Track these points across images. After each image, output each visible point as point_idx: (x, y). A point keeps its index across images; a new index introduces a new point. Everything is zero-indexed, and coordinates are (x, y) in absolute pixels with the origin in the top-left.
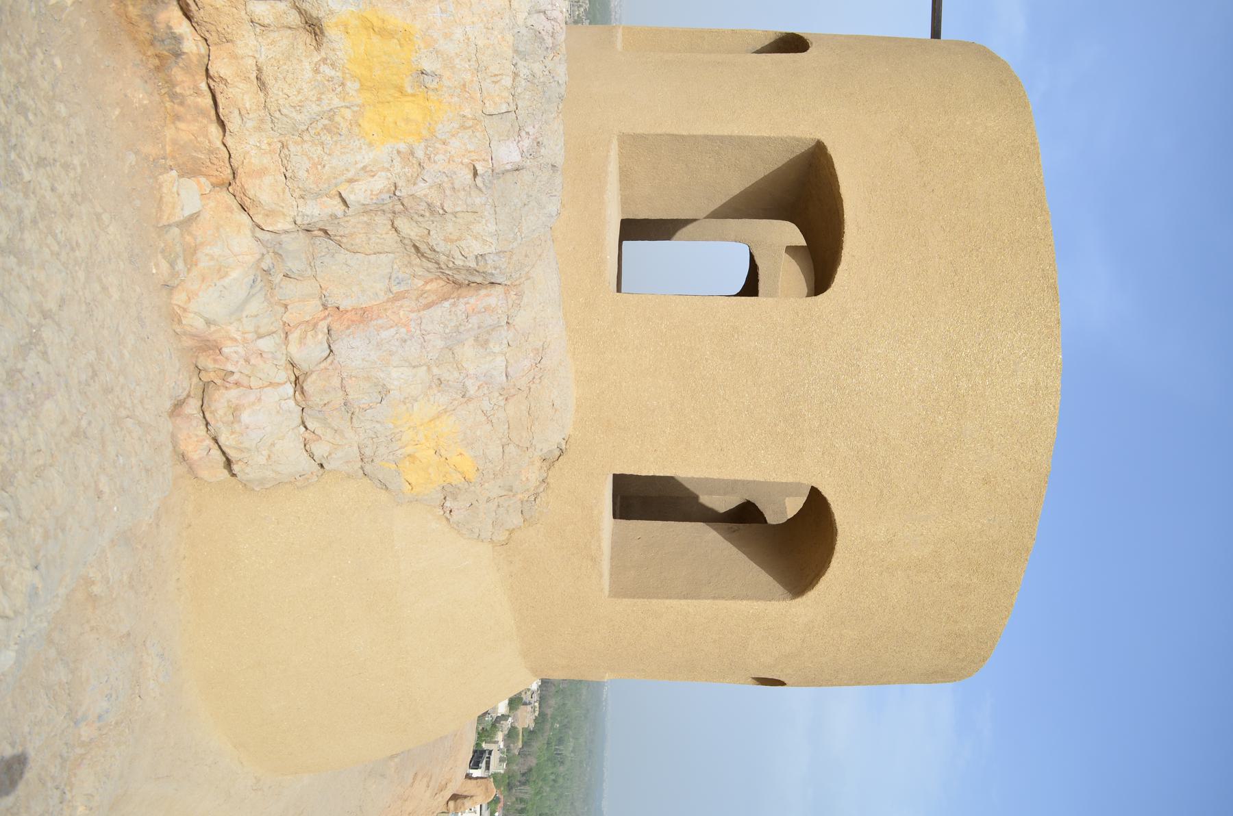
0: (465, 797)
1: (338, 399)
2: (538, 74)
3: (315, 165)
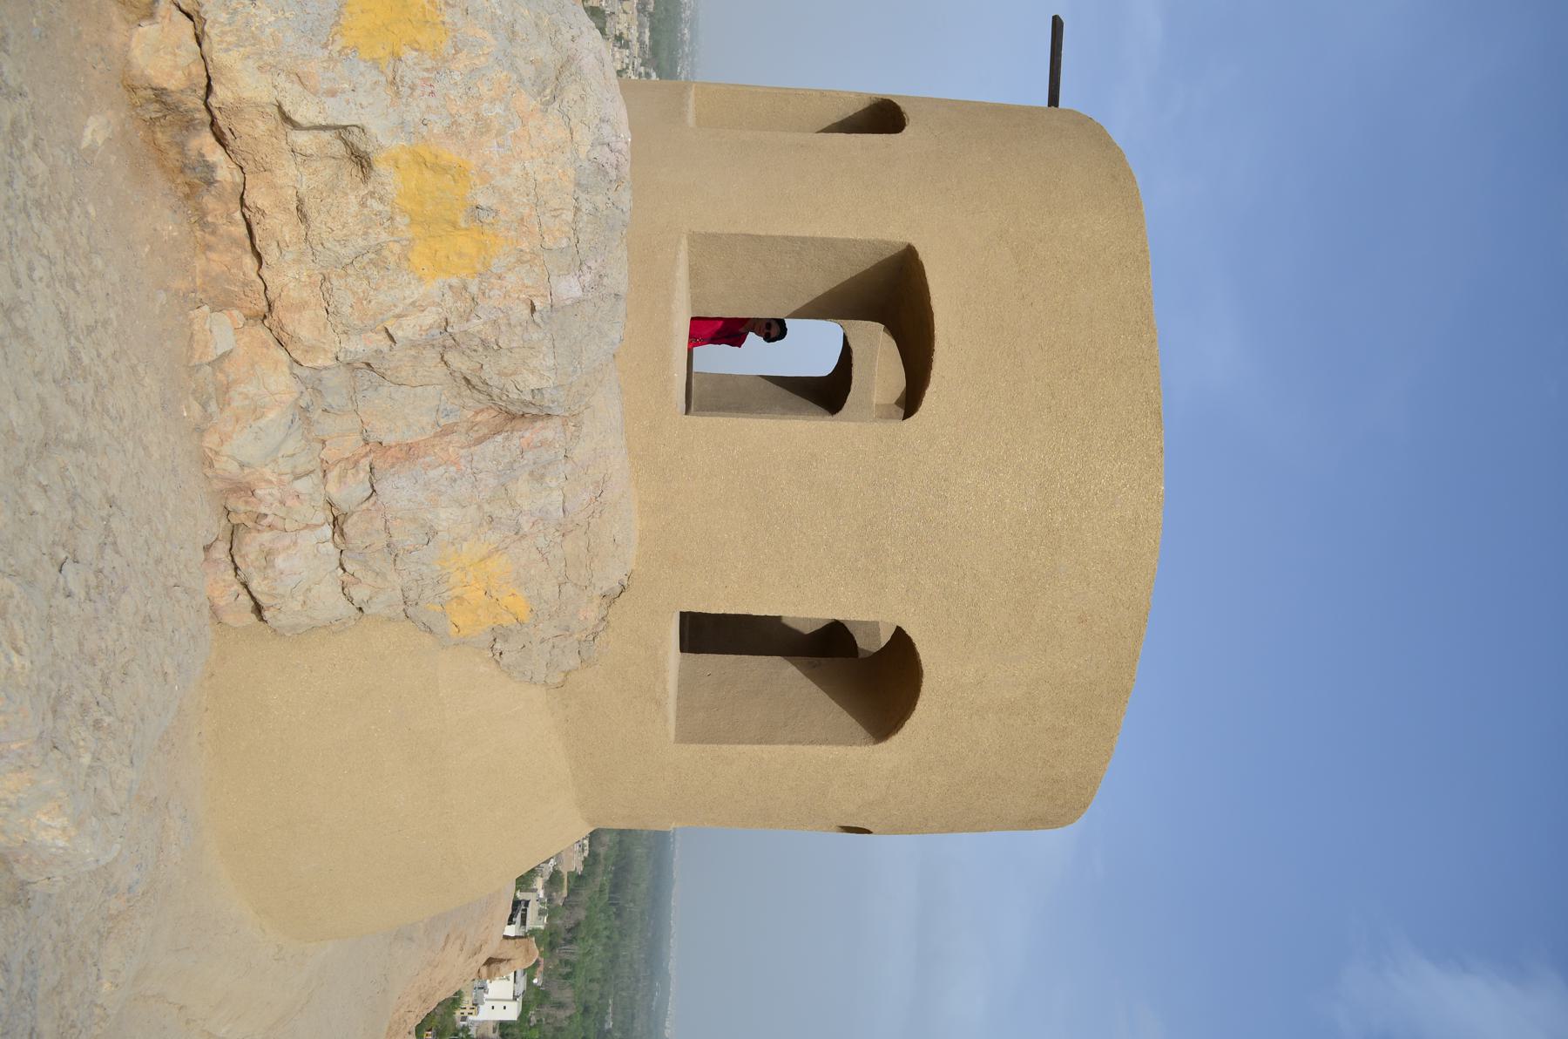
0: (501, 961)
1: (381, 541)
2: (601, 206)
3: (360, 300)
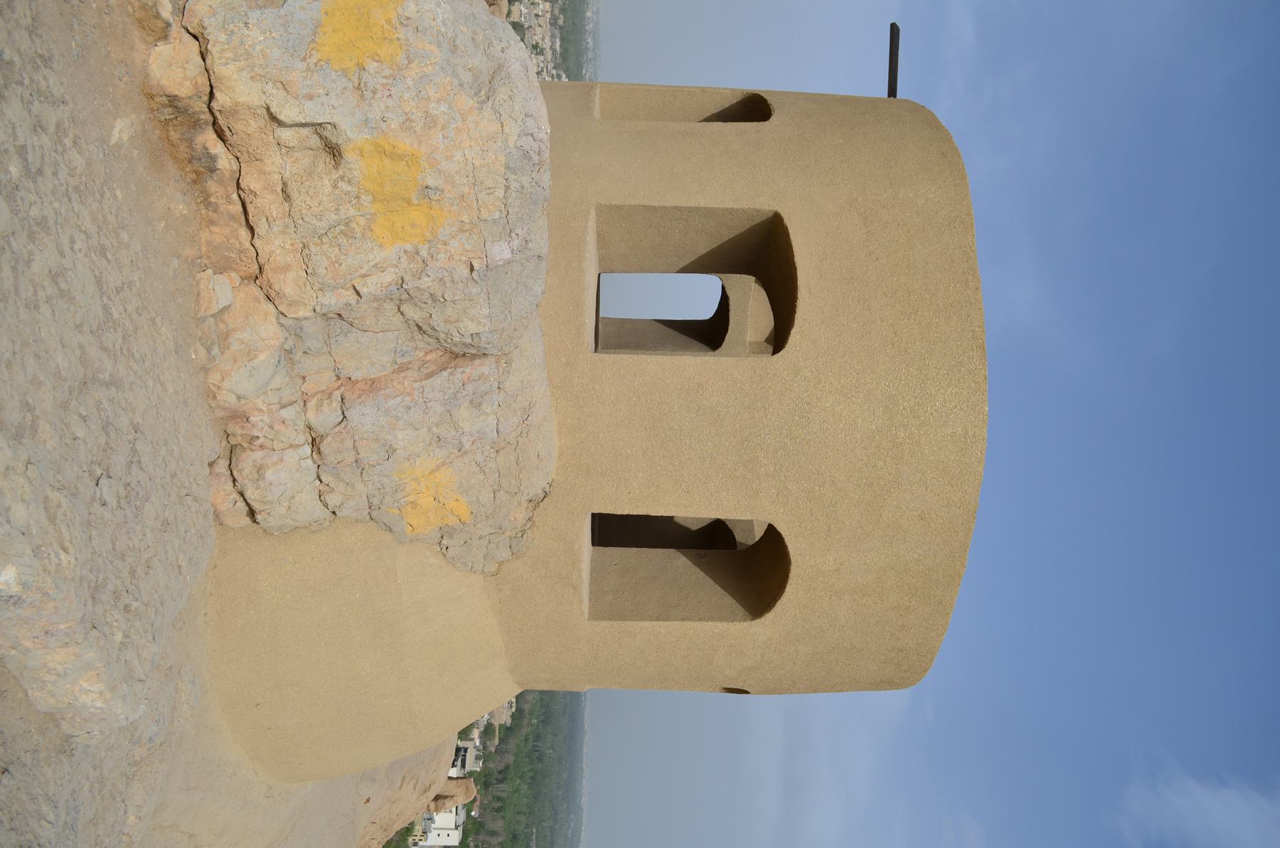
0: (446, 797)
2: (527, 185)
3: (333, 263)
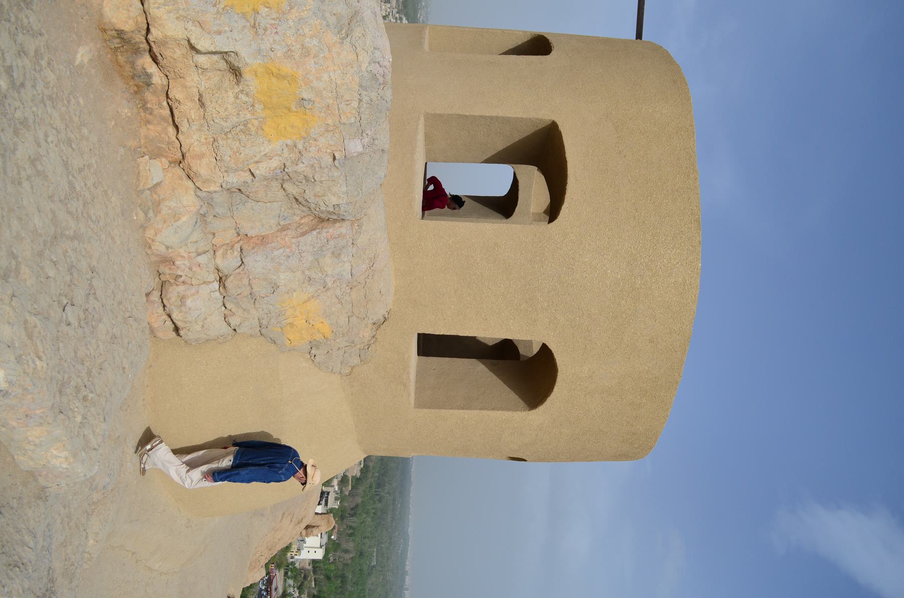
0: (314, 527)
1: (247, 291)
2: (374, 99)
3: (235, 153)
